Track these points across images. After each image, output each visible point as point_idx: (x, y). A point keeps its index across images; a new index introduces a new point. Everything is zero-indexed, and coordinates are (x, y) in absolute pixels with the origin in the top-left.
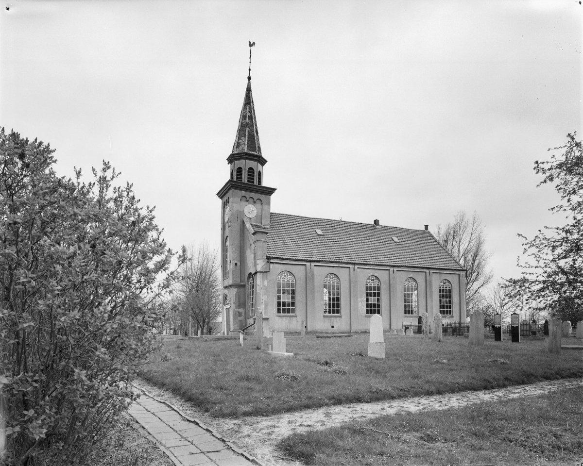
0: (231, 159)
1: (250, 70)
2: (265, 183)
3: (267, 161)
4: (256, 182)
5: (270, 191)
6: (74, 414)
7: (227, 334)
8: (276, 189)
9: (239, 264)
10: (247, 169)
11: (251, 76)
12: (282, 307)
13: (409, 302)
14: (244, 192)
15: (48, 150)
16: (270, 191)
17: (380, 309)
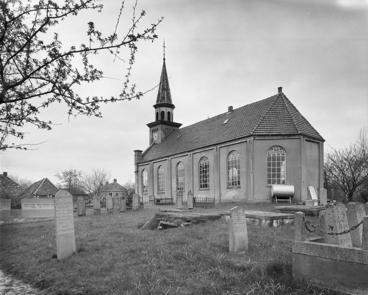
1: (164, 55)
2: (175, 121)
3: (7, 172)
4: (171, 121)
10: (167, 112)
11: (130, 72)
12: (272, 179)
13: (203, 170)
17: (200, 179)
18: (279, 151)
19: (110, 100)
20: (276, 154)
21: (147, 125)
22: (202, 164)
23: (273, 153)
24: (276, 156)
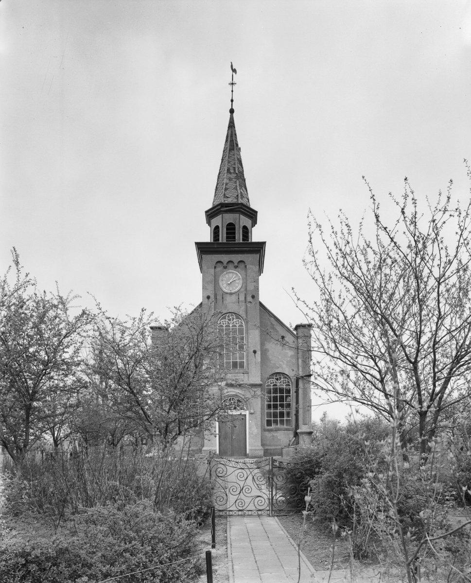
0: (211, 215)
1: (232, 101)
7: (222, 241)
9: (212, 297)
11: (233, 108)
12: (279, 419)
19: (232, 107)
20: (231, 326)
21: (196, 243)
23: (226, 323)
24: (224, 328)
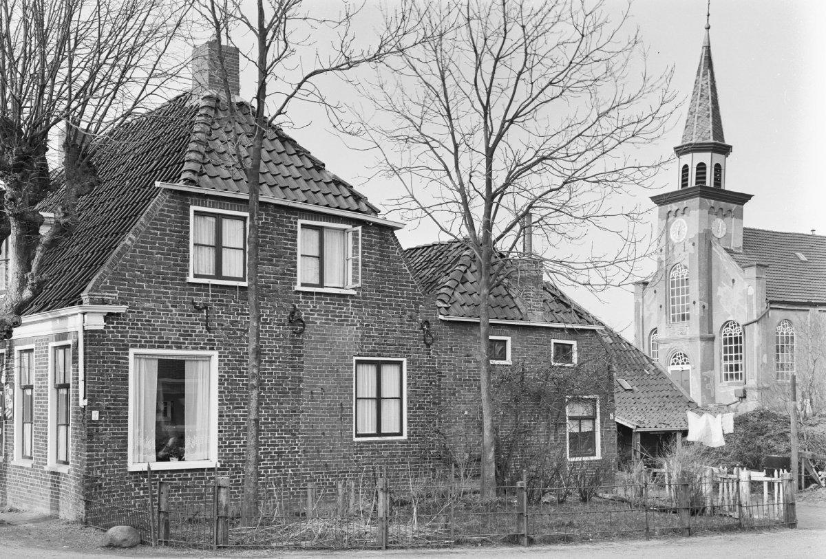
2: (730, 184)
3: (731, 147)
5: (742, 199)
6: (248, 172)
8: (752, 196)
14: (713, 201)
15: (324, 165)
16: (742, 199)
18: (683, 359)
22: (728, 334)
